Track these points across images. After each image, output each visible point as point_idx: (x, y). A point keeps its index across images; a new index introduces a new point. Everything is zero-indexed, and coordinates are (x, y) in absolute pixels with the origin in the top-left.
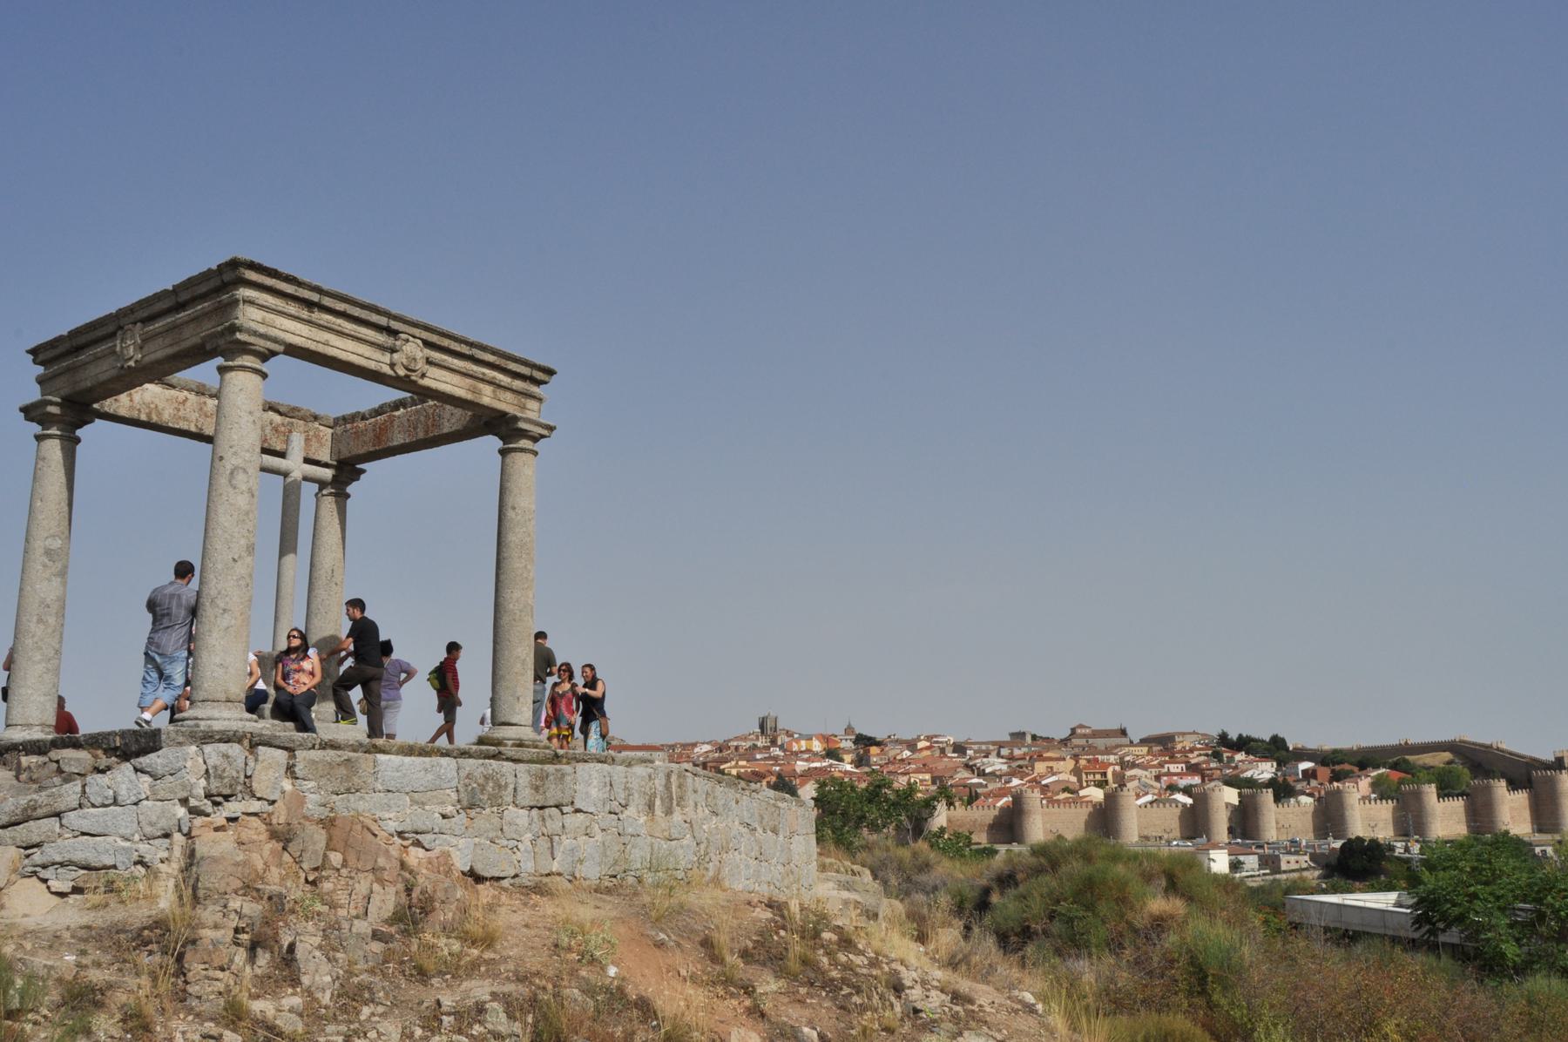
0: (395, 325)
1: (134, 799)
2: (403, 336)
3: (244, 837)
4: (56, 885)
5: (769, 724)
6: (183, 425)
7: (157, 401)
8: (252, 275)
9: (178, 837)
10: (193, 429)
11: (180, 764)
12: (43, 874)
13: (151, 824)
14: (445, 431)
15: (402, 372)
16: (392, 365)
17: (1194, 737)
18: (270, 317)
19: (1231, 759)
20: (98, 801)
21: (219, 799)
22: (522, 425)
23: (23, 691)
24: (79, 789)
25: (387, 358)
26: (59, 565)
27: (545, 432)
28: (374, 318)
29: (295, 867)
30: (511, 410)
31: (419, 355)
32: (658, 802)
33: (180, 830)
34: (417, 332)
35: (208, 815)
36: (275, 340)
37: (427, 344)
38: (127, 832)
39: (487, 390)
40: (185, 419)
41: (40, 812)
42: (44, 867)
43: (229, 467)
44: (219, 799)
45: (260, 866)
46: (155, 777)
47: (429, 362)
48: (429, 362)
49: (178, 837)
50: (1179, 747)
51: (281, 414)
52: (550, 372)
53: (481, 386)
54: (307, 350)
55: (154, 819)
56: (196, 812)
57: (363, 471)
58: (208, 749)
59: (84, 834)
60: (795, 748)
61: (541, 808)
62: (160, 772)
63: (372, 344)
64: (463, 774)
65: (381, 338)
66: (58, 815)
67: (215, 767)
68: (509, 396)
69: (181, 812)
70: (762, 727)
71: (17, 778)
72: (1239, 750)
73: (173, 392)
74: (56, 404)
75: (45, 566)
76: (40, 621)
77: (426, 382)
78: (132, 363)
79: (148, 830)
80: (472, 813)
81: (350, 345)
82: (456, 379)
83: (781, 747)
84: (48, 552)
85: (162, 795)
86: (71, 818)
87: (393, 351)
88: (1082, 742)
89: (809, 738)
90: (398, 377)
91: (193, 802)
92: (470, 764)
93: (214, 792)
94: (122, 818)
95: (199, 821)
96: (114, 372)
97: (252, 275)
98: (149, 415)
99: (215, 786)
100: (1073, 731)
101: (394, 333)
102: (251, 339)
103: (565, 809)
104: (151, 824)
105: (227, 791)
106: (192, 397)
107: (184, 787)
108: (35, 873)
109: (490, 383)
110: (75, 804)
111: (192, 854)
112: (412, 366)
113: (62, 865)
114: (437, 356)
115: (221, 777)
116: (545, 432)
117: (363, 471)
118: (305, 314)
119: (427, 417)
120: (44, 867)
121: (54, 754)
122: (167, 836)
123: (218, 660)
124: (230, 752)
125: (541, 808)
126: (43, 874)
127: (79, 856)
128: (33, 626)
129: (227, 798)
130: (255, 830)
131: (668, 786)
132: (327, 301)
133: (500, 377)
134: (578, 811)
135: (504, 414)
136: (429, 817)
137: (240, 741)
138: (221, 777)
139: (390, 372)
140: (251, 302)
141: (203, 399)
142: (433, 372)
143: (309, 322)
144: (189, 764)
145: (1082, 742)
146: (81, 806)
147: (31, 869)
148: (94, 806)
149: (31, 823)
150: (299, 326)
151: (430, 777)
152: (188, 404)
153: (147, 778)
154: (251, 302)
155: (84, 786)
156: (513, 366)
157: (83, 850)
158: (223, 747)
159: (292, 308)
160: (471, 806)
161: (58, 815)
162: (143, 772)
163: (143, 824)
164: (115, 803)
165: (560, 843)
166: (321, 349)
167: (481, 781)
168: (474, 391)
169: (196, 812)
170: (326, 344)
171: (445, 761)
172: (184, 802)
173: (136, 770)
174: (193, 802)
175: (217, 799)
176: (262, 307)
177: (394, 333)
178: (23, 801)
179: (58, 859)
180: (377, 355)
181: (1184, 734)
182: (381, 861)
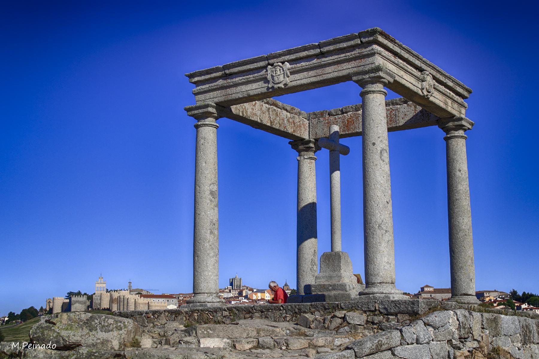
0: (424, 67)
5: (236, 283)
8: (380, 39)
13: (437, 354)
14: (401, 124)
15: (426, 93)
16: (422, 89)
17: (496, 294)
19: (519, 308)
21: (463, 340)
23: (206, 273)
27: (470, 127)
37: (434, 78)
39: (449, 102)
40: (256, 115)
41: (384, 347)
43: (379, 149)
46: (435, 328)
50: (487, 299)
60: (254, 297)
65: (418, 74)
67: (462, 323)
70: (231, 284)
72: (523, 303)
74: (213, 107)
75: (211, 201)
76: (211, 233)
77: (432, 99)
83: (246, 297)
88: (428, 296)
89: (262, 291)
90: (424, 96)
96: (264, 90)
97: (380, 39)
100: (422, 289)
101: (421, 70)
104: (437, 354)
107: (449, 333)
109: (451, 98)
118: (392, 58)
128: (208, 235)
142: (436, 94)
144: (451, 321)
145: (428, 296)
146: (401, 344)
148: (408, 344)
149: (380, 354)
153: (431, 329)
162: (428, 325)
168: (446, 104)
172: (450, 341)
173: (426, 324)
176: (383, 57)
181: (489, 292)
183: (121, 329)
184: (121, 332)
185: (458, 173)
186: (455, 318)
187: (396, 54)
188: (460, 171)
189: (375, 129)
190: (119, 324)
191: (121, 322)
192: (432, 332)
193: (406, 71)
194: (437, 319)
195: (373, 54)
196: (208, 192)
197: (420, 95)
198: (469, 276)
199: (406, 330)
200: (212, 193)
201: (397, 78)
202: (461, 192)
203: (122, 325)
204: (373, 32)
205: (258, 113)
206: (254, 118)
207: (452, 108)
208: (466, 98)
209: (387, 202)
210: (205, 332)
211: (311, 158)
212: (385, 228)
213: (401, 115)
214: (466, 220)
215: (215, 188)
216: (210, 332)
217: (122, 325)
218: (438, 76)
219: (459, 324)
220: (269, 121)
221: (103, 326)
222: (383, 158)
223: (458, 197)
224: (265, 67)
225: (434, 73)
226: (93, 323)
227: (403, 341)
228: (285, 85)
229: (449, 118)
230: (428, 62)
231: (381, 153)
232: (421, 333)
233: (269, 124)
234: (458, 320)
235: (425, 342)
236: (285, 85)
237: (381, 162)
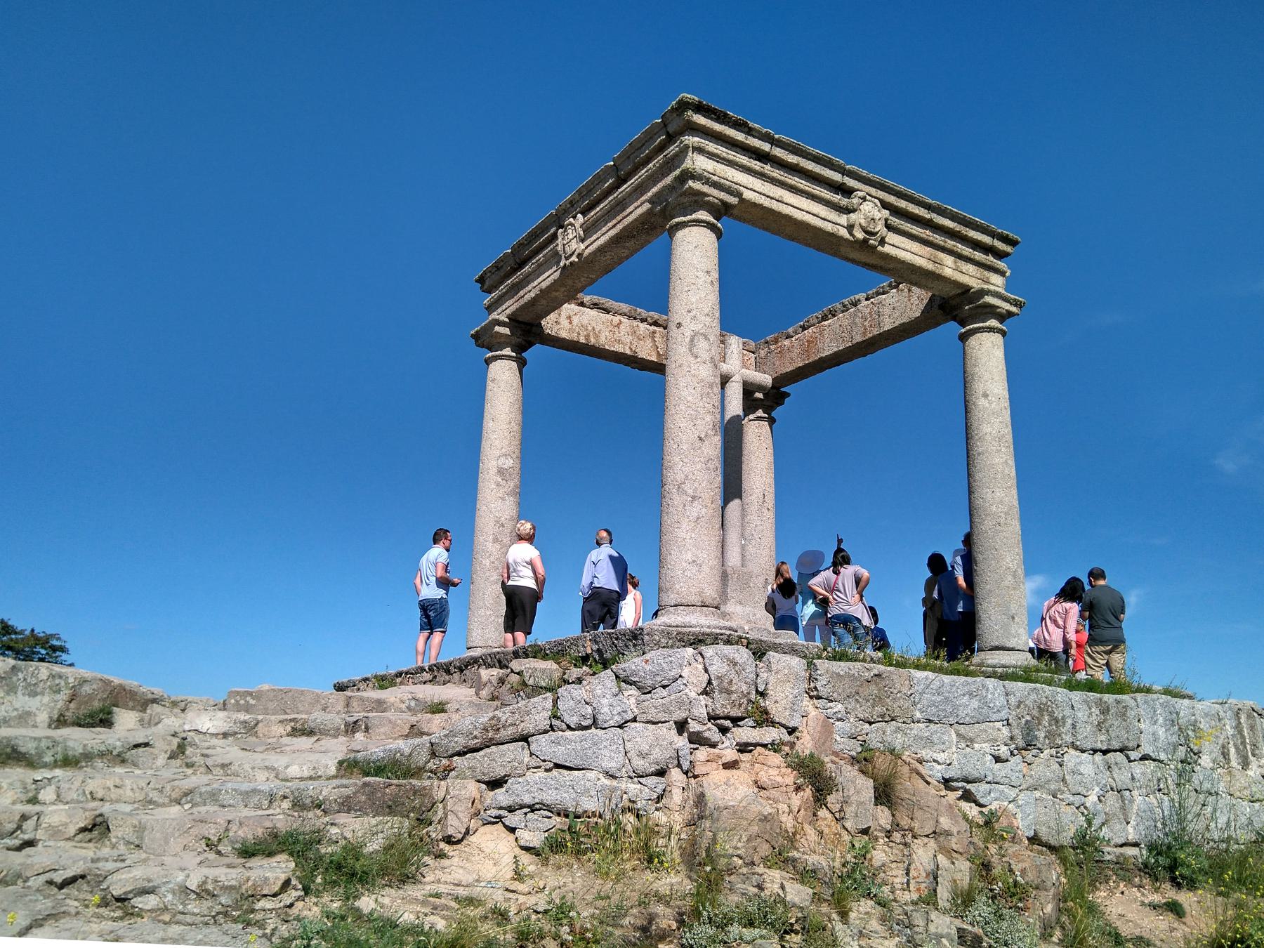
0: (851, 183)
1: (618, 719)
3: (764, 778)
4: (527, 837)
7: (593, 324)
8: (700, 119)
9: (676, 775)
11: (674, 673)
12: (512, 820)
13: (642, 755)
15: (860, 235)
16: (850, 228)
20: (573, 721)
21: (728, 723)
22: (989, 299)
24: (549, 704)
25: (843, 219)
27: (1014, 309)
29: (836, 827)
30: (975, 284)
32: (1232, 750)
33: (679, 765)
35: (714, 746)
37: (885, 205)
38: (611, 765)
39: (949, 260)
40: (619, 342)
42: (511, 810)
43: (688, 334)
44: (728, 723)
45: (788, 822)
48: (889, 227)
49: (676, 775)
52: (1013, 243)
53: (941, 255)
55: (645, 748)
56: (697, 740)
57: (787, 395)
58: (709, 651)
59: (557, 766)
61: (1105, 752)
64: (1013, 700)
65: (836, 198)
66: (524, 739)
68: (971, 268)
69: (682, 742)
71: (477, 694)
75: (498, 485)
77: (887, 249)
78: (574, 258)
79: (639, 763)
80: (1029, 755)
82: (916, 247)
84: (501, 471)
85: (653, 714)
86: (541, 744)
87: (848, 210)
90: (857, 241)
91: (694, 726)
92: (1019, 688)
93: (719, 712)
94: (606, 750)
95: (703, 753)
97: (700, 119)
98: (587, 337)
99: (722, 705)
101: (847, 192)
102: (706, 189)
103: (1134, 755)
104: (642, 755)
105: (736, 713)
106: (625, 320)
107: (681, 705)
108: (500, 817)
110: (545, 724)
111: (701, 799)
113: (532, 808)
114: (895, 221)
115: (729, 693)
116: (1014, 309)
117: (787, 395)
120: (511, 810)
121: (516, 665)
122: (661, 773)
123: (689, 557)
125: (1105, 752)
126: (512, 820)
127: (550, 797)
129: (736, 721)
130: (775, 770)
131: (1238, 727)
132: (778, 152)
133: (960, 247)
134: (1145, 758)
135: (966, 289)
136: (977, 760)
138: (729, 693)
139: (847, 235)
140: (700, 150)
141: (635, 323)
142: (892, 238)
147: (494, 812)
148: (569, 727)
150: (751, 179)
151: (975, 703)
153: (633, 691)
155: (555, 702)
156: (973, 234)
157: (559, 789)
158: (729, 650)
160: (1028, 746)
161: (524, 739)
163: (631, 754)
164: (595, 723)
165: (1132, 801)
167: (1035, 713)
169: (697, 740)
171: (991, 682)
172: (681, 726)
174: (694, 726)
175: (725, 723)
177: (847, 192)
178: (484, 719)
179: (527, 799)
180: (833, 216)
182: (945, 823)
183: (59, 691)
184: (58, 697)
185: (982, 402)
186: (700, 667)
187: (976, 245)
188: (986, 396)
189: (683, 296)
190: (57, 681)
191: (60, 677)
192: (633, 700)
193: (731, 164)
194: (648, 667)
195: (684, 150)
196: (493, 471)
197: (847, 240)
198: (1008, 609)
199: (565, 694)
200: (501, 471)
201: (748, 195)
202: (988, 438)
203: (63, 683)
204: (683, 106)
205: (628, 339)
206: (618, 348)
207: (969, 276)
208: (1006, 255)
209: (700, 439)
210: (242, 702)
211: (759, 418)
212: (690, 492)
213: (887, 311)
214: (999, 494)
215: (508, 463)
216: (252, 702)
217: (63, 683)
218: (891, 199)
219: (710, 682)
220: (654, 353)
221: (30, 685)
222: (695, 350)
223: (980, 450)
224: (555, 236)
225: (881, 194)
226: (15, 679)
227: (556, 721)
228: (579, 255)
229: (959, 294)
230: (864, 172)
231: (692, 340)
232: (605, 701)
233: (654, 359)
234: (706, 671)
235: (612, 723)
236: (579, 255)
237: (691, 359)
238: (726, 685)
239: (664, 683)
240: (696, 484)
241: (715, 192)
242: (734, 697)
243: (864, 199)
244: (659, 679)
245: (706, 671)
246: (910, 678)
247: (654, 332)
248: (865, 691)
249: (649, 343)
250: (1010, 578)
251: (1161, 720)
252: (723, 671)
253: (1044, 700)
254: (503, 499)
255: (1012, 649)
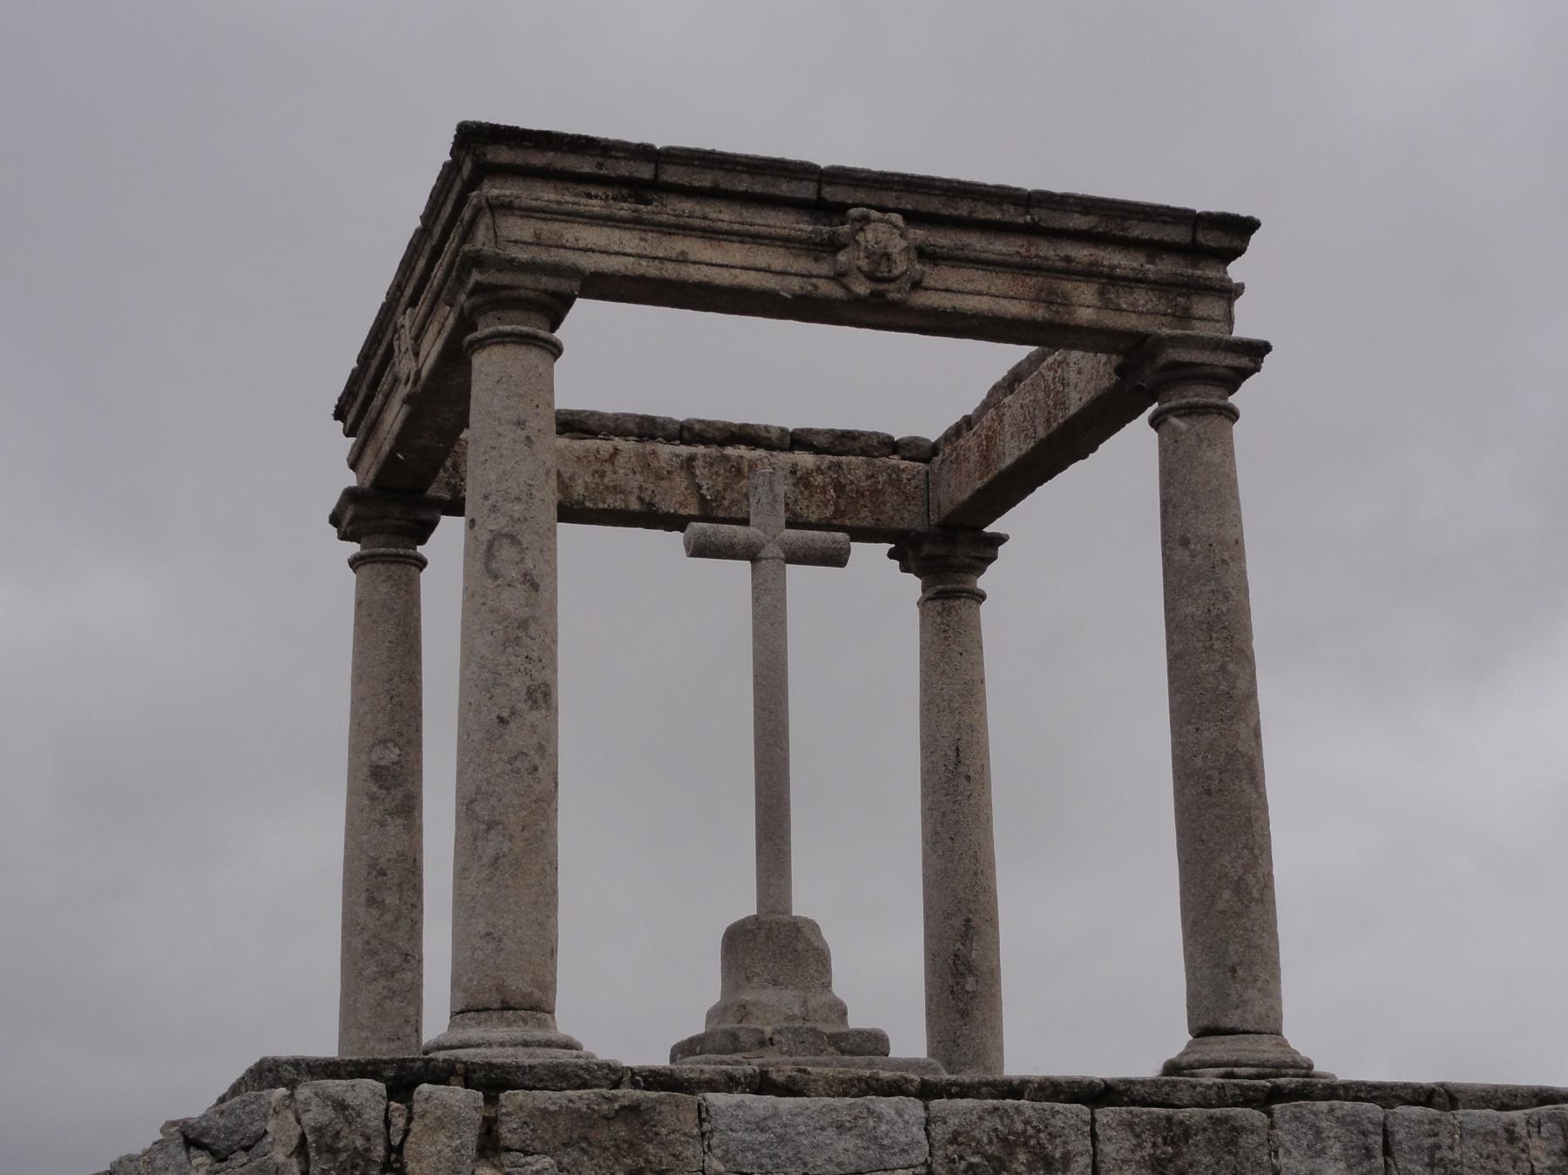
2: (854, 212)
6: (613, 502)
10: (635, 505)
15: (862, 288)
16: (839, 277)
18: (550, 229)
26: (398, 794)
27: (1244, 362)
28: (785, 188)
31: (897, 244)
34: (889, 199)
36: (556, 270)
37: (913, 218)
40: (616, 489)
47: (925, 254)
48: (925, 254)
51: (817, 451)
54: (643, 279)
57: (1000, 539)
62: (222, 1145)
63: (786, 242)
65: (803, 226)
67: (319, 1130)
68: (1142, 298)
73: (591, 444)
81: (736, 253)
82: (1001, 283)
87: (834, 246)
97: (504, 155)
102: (507, 279)
106: (627, 446)
109: (1090, 273)
112: (883, 271)
114: (944, 239)
115: (333, 1151)
116: (1244, 362)
117: (1000, 539)
118: (624, 209)
119: (1047, 391)
124: (349, 1098)
137: (375, 1075)
138: (333, 1151)
141: (649, 446)
143: (636, 223)
151: (850, 1142)
152: (620, 460)
154: (503, 207)
159: (568, 198)
166: (670, 271)
170: (682, 259)
176: (529, 212)
177: (840, 209)
209: (501, 720)
234: (298, 1121)
238: (329, 1140)
239: (245, 1143)
240: (493, 801)
241: (527, 280)
242: (343, 1156)
243: (865, 219)
244: (236, 1138)
245: (298, 1121)
246: (702, 1113)
247: (692, 458)
248: (602, 1134)
249: (681, 482)
250: (1227, 895)
251: (1336, 1149)
252: (324, 1119)
253: (1019, 1126)
254: (382, 824)
255: (1232, 1032)
